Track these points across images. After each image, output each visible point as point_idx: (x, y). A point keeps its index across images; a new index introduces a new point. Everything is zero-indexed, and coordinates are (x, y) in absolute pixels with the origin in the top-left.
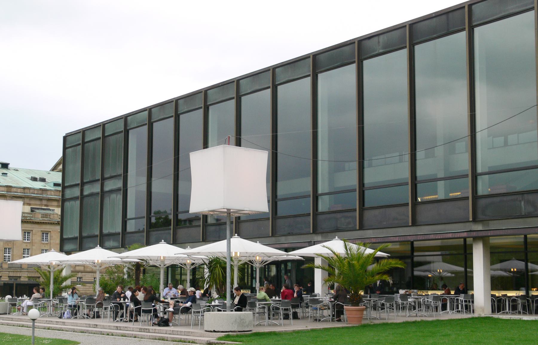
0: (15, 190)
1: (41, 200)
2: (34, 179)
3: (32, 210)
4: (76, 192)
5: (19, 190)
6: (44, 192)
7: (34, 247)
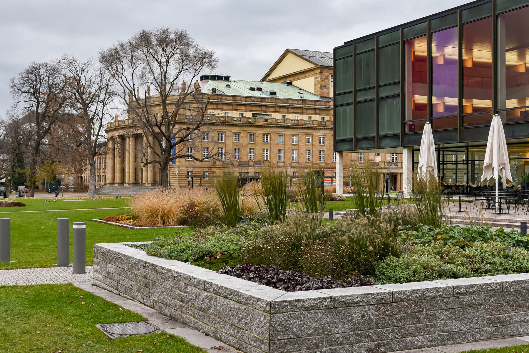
0: (239, 98)
1: (260, 106)
2: (252, 89)
3: (254, 116)
4: (350, 99)
5: (242, 99)
6: (263, 100)
7: (257, 147)
